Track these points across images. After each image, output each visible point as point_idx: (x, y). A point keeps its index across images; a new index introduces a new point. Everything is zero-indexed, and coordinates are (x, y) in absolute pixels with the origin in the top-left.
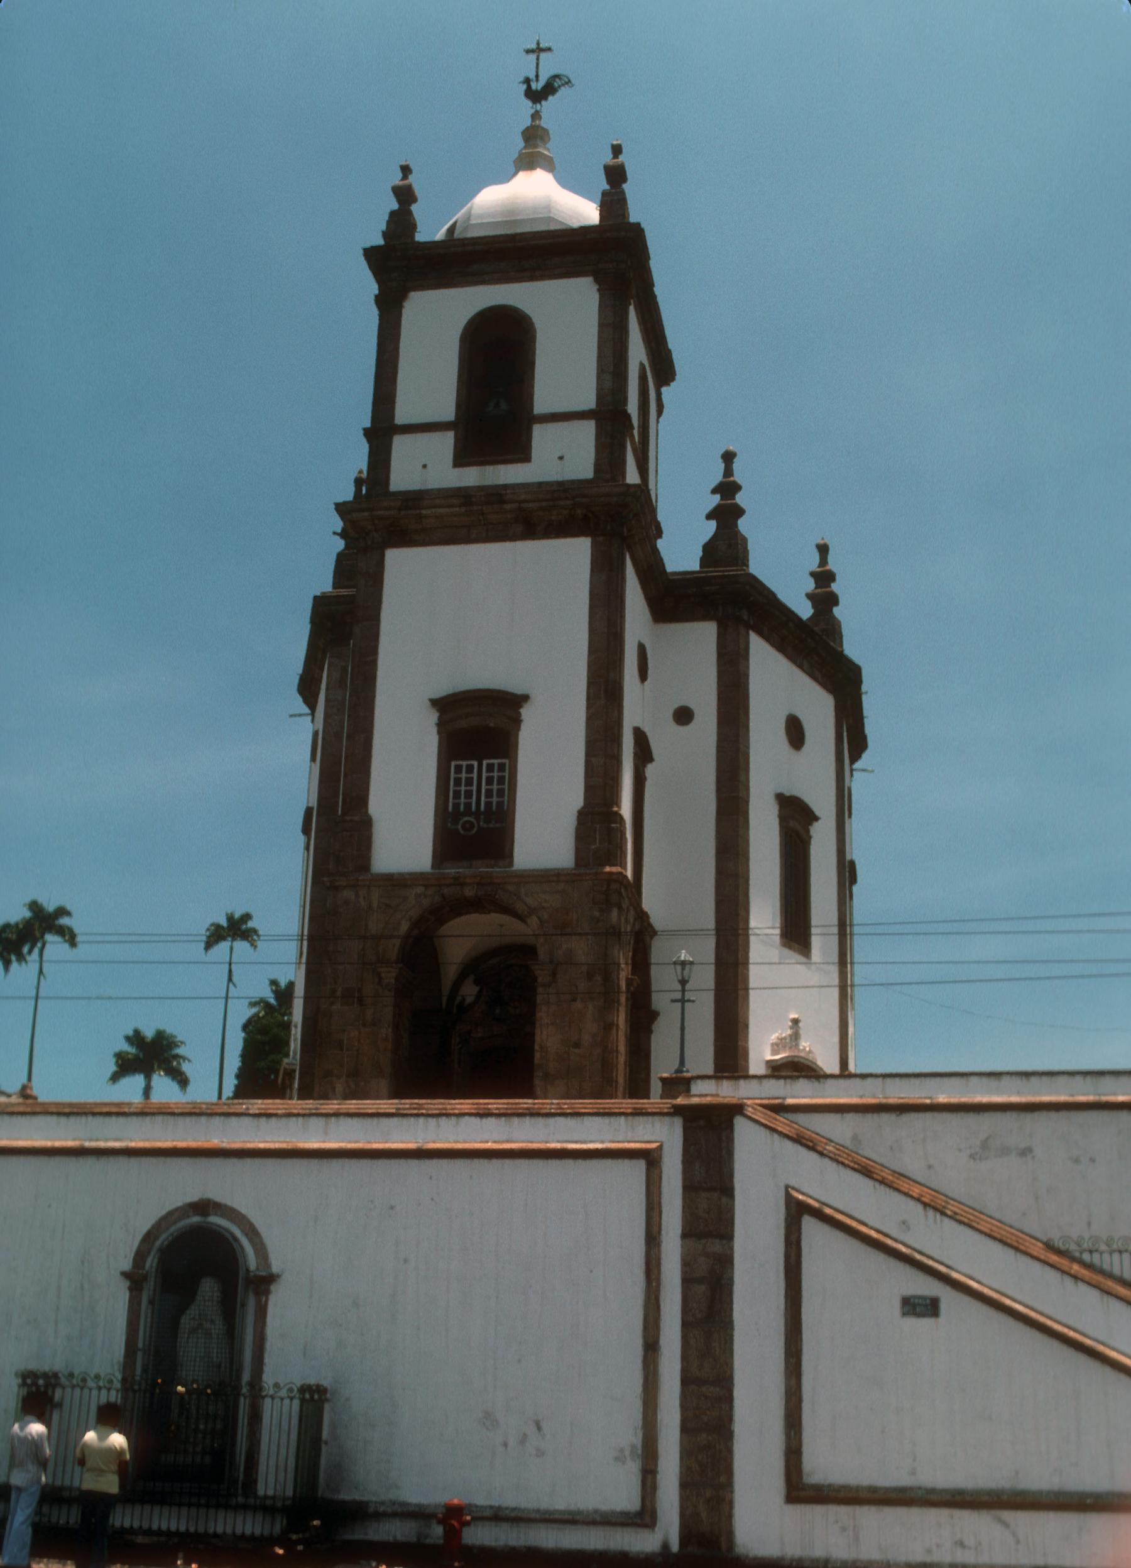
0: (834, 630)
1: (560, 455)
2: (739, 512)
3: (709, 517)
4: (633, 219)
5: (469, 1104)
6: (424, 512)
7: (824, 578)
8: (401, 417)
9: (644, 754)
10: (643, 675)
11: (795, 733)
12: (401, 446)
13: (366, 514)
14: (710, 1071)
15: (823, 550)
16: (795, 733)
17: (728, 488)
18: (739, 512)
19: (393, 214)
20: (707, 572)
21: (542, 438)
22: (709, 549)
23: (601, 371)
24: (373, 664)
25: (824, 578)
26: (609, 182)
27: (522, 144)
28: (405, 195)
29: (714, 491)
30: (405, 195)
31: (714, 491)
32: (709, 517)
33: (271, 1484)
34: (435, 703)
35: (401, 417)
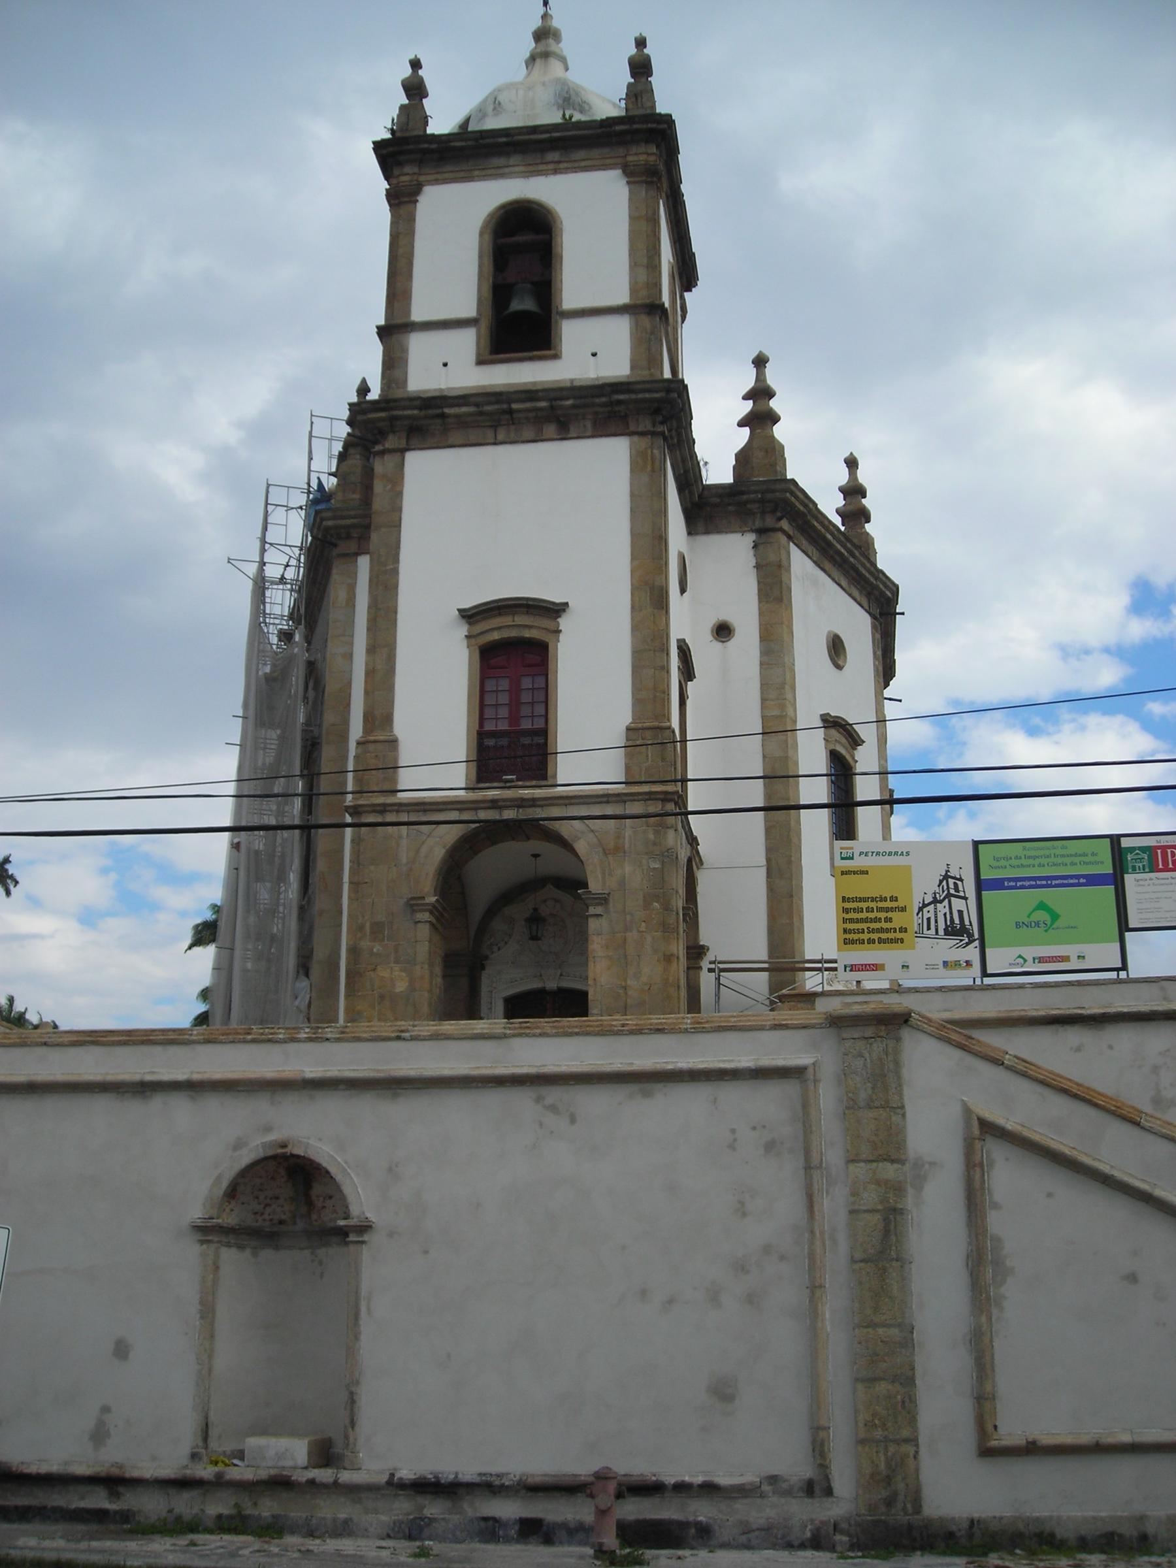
0: (865, 547)
1: (594, 351)
2: (774, 419)
3: (741, 424)
4: (661, 109)
5: (1040, 1073)
6: (447, 411)
7: (853, 491)
8: (418, 313)
9: (688, 672)
10: (683, 590)
11: (836, 648)
12: (419, 346)
13: (383, 414)
14: (1125, 972)
15: (852, 463)
16: (836, 648)
17: (760, 393)
18: (774, 419)
19: (403, 108)
20: (494, 804)
21: (570, 333)
22: (743, 458)
23: (634, 265)
24: (395, 572)
25: (853, 491)
26: (633, 75)
27: (533, 45)
28: (415, 89)
29: (746, 398)
30: (415, 89)
31: (746, 398)
32: (741, 424)
33: (296, 802)
34: (469, 616)
35: (418, 313)
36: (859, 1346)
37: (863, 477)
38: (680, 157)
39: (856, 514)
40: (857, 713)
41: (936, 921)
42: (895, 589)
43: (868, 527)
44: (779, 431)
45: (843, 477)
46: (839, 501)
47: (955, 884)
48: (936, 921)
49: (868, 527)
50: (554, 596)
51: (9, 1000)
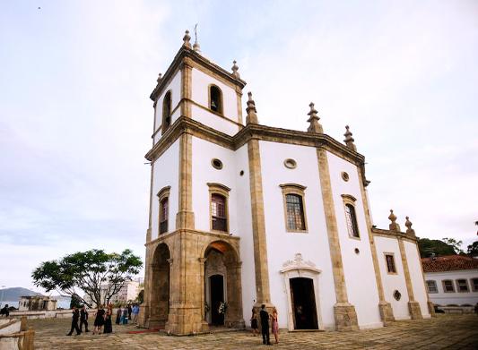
0: (353, 148)
7: (348, 134)
11: (345, 176)
16: (345, 176)
25: (348, 134)
36: (197, 262)
37: (350, 130)
38: (431, 239)
39: (350, 141)
40: (357, 193)
41: (404, 259)
42: (363, 157)
43: (354, 143)
44: (412, 227)
45: (345, 131)
46: (345, 138)
47: (215, 94)
48: (404, 259)
49: (354, 143)
50: (304, 185)
51: (215, 196)
